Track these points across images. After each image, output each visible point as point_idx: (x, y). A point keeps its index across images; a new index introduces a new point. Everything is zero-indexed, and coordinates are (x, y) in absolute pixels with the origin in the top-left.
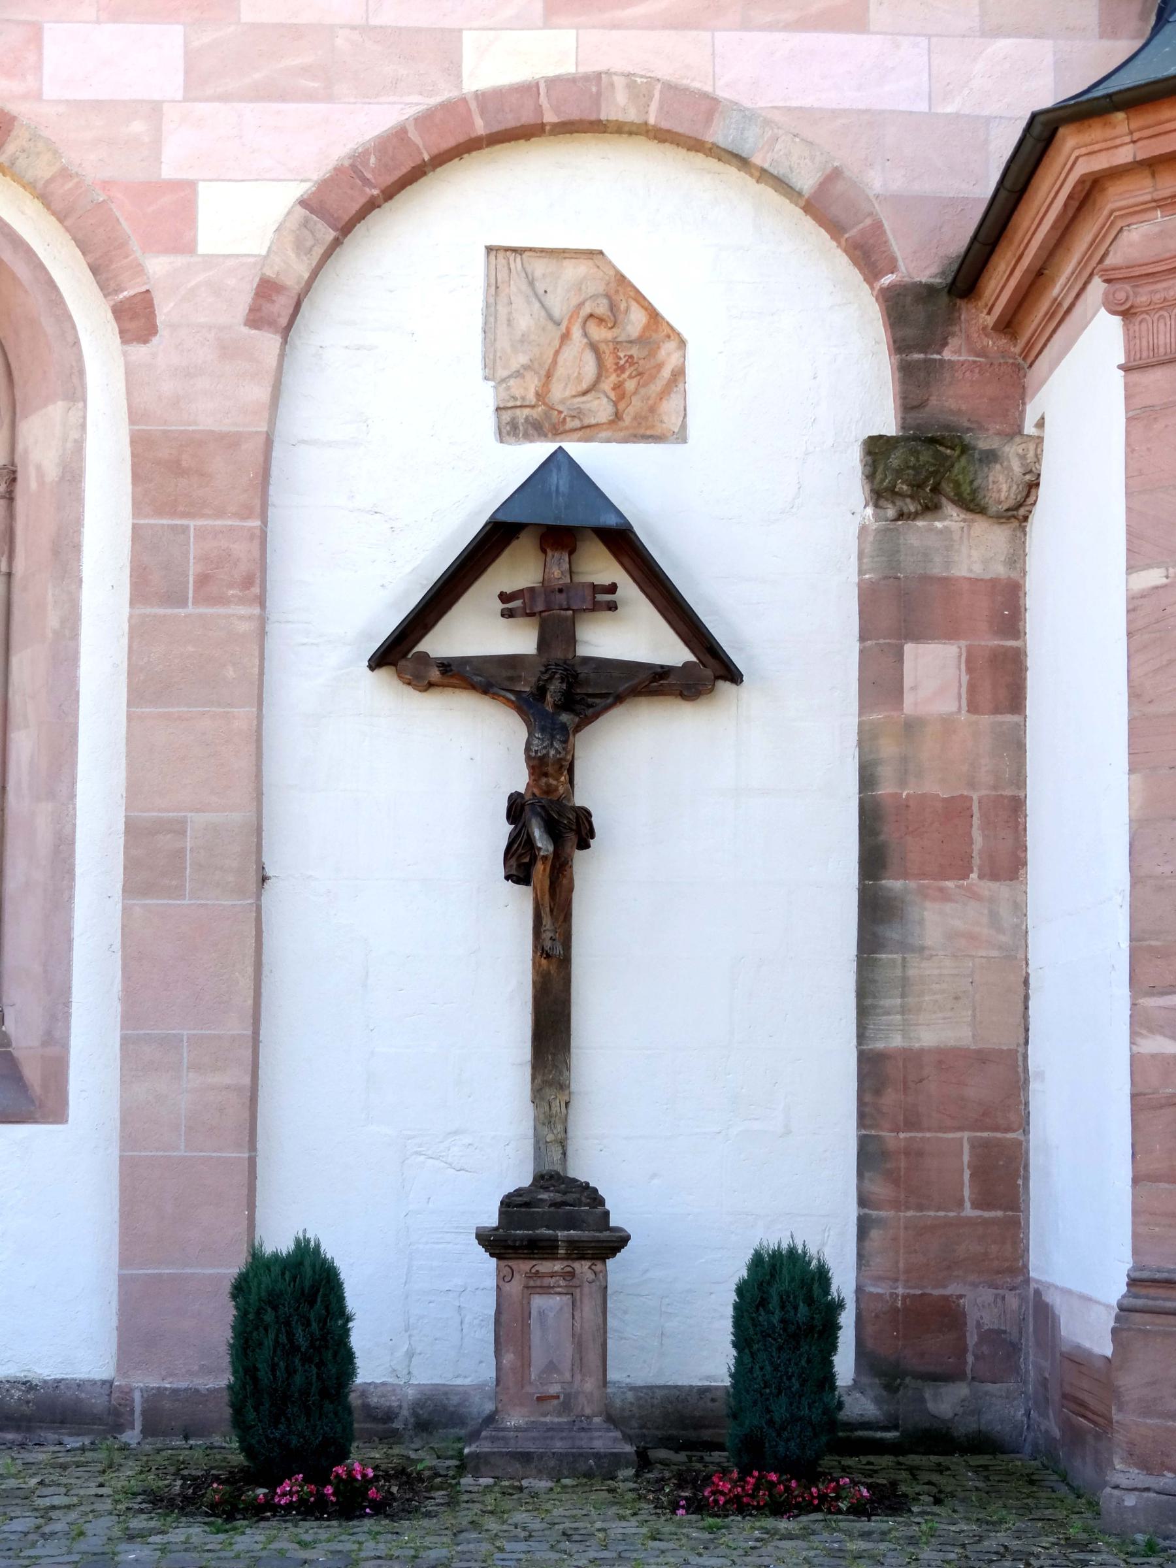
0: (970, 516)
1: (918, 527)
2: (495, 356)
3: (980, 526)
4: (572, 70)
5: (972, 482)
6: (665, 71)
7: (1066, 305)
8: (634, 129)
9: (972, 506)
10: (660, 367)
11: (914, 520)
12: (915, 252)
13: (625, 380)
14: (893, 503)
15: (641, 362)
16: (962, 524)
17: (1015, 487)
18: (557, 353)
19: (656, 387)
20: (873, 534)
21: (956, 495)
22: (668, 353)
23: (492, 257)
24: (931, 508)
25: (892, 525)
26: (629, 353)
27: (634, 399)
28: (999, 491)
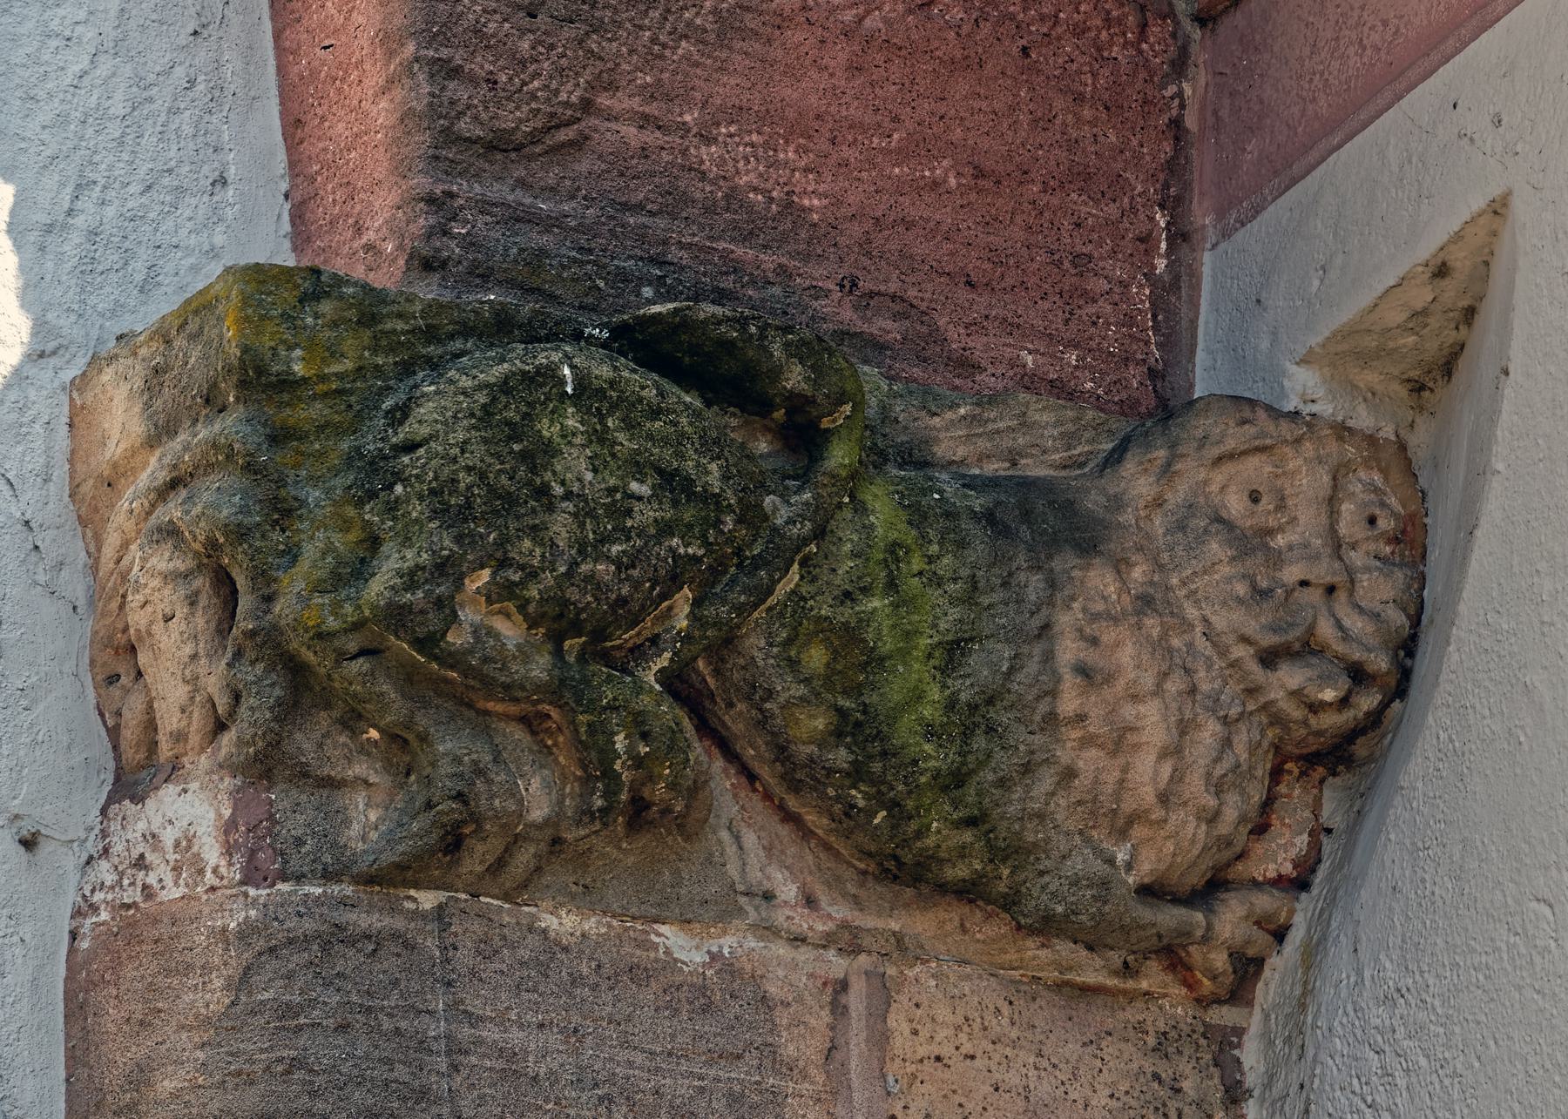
1: (553, 947)
8: (225, 591)
9: (939, 831)
16: (836, 964)
17: (1210, 731)
20: (226, 964)
21: (845, 728)
28: (1120, 741)
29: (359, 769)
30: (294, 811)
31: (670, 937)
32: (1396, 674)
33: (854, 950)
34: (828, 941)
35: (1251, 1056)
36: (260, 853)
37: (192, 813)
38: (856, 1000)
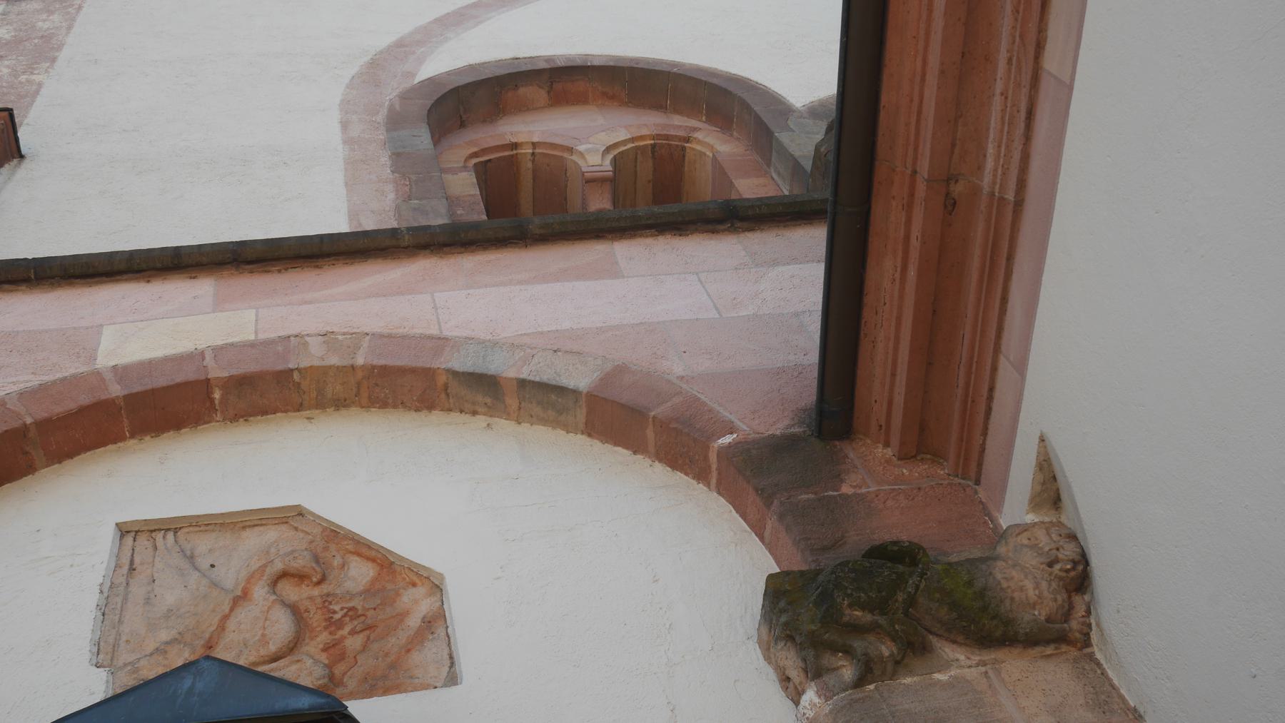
0: (989, 656)
1: (908, 686)
2: (117, 640)
3: (1014, 664)
4: (252, 337)
5: (970, 583)
6: (375, 326)
7: (1010, 196)
10: (402, 616)
11: (893, 676)
12: (754, 412)
13: (343, 638)
14: (848, 652)
15: (371, 613)
16: (983, 669)
18: (226, 618)
19: (402, 637)
22: (417, 604)
23: (129, 540)
24: (914, 648)
25: (858, 694)
26: (351, 605)
27: (361, 659)
29: (841, 663)
30: (830, 679)
31: (937, 676)
32: (1083, 560)
33: (985, 665)
34: (978, 665)
35: (1099, 656)
36: (826, 693)
37: (810, 695)
38: (991, 674)
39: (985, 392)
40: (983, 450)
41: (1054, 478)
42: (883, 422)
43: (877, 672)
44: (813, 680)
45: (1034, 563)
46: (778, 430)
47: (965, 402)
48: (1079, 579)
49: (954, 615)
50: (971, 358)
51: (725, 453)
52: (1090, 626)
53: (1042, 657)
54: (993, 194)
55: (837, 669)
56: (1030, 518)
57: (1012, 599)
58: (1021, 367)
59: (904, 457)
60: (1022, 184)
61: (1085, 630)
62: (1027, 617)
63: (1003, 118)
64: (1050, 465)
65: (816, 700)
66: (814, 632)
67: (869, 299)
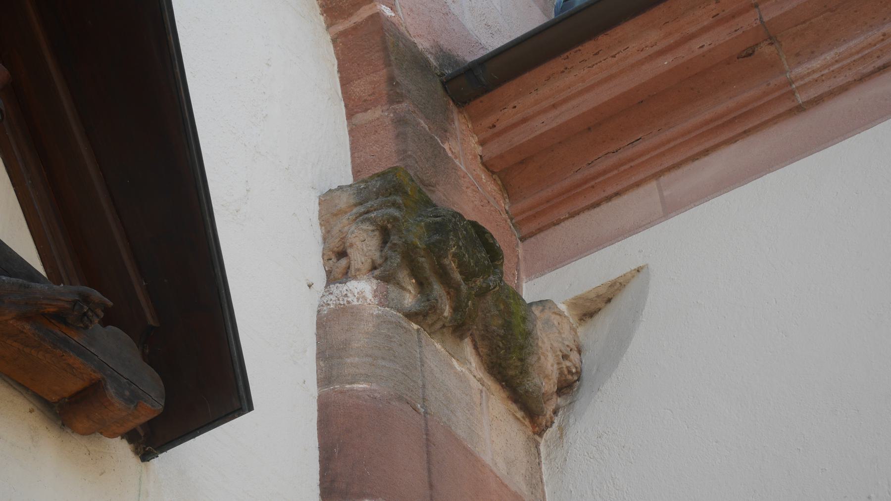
0: (489, 382)
7: (801, 98)
14: (422, 285)
24: (459, 329)
25: (404, 322)
29: (410, 288)
35: (542, 448)
38: (484, 394)
39: (610, 191)
40: (557, 223)
41: (609, 300)
42: (500, 126)
43: (429, 320)
44: (377, 278)
45: (555, 345)
46: (423, 44)
47: (586, 181)
48: (567, 386)
49: (502, 332)
50: (631, 160)
51: (377, 17)
52: (552, 422)
53: (514, 415)
54: (790, 83)
55: (403, 288)
56: (563, 307)
57: (539, 359)
58: (671, 208)
59: (487, 166)
60: (817, 101)
61: (549, 424)
62: (537, 381)
63: (863, 49)
64: (619, 290)
65: (369, 296)
66: (417, 247)
67: (603, 40)
